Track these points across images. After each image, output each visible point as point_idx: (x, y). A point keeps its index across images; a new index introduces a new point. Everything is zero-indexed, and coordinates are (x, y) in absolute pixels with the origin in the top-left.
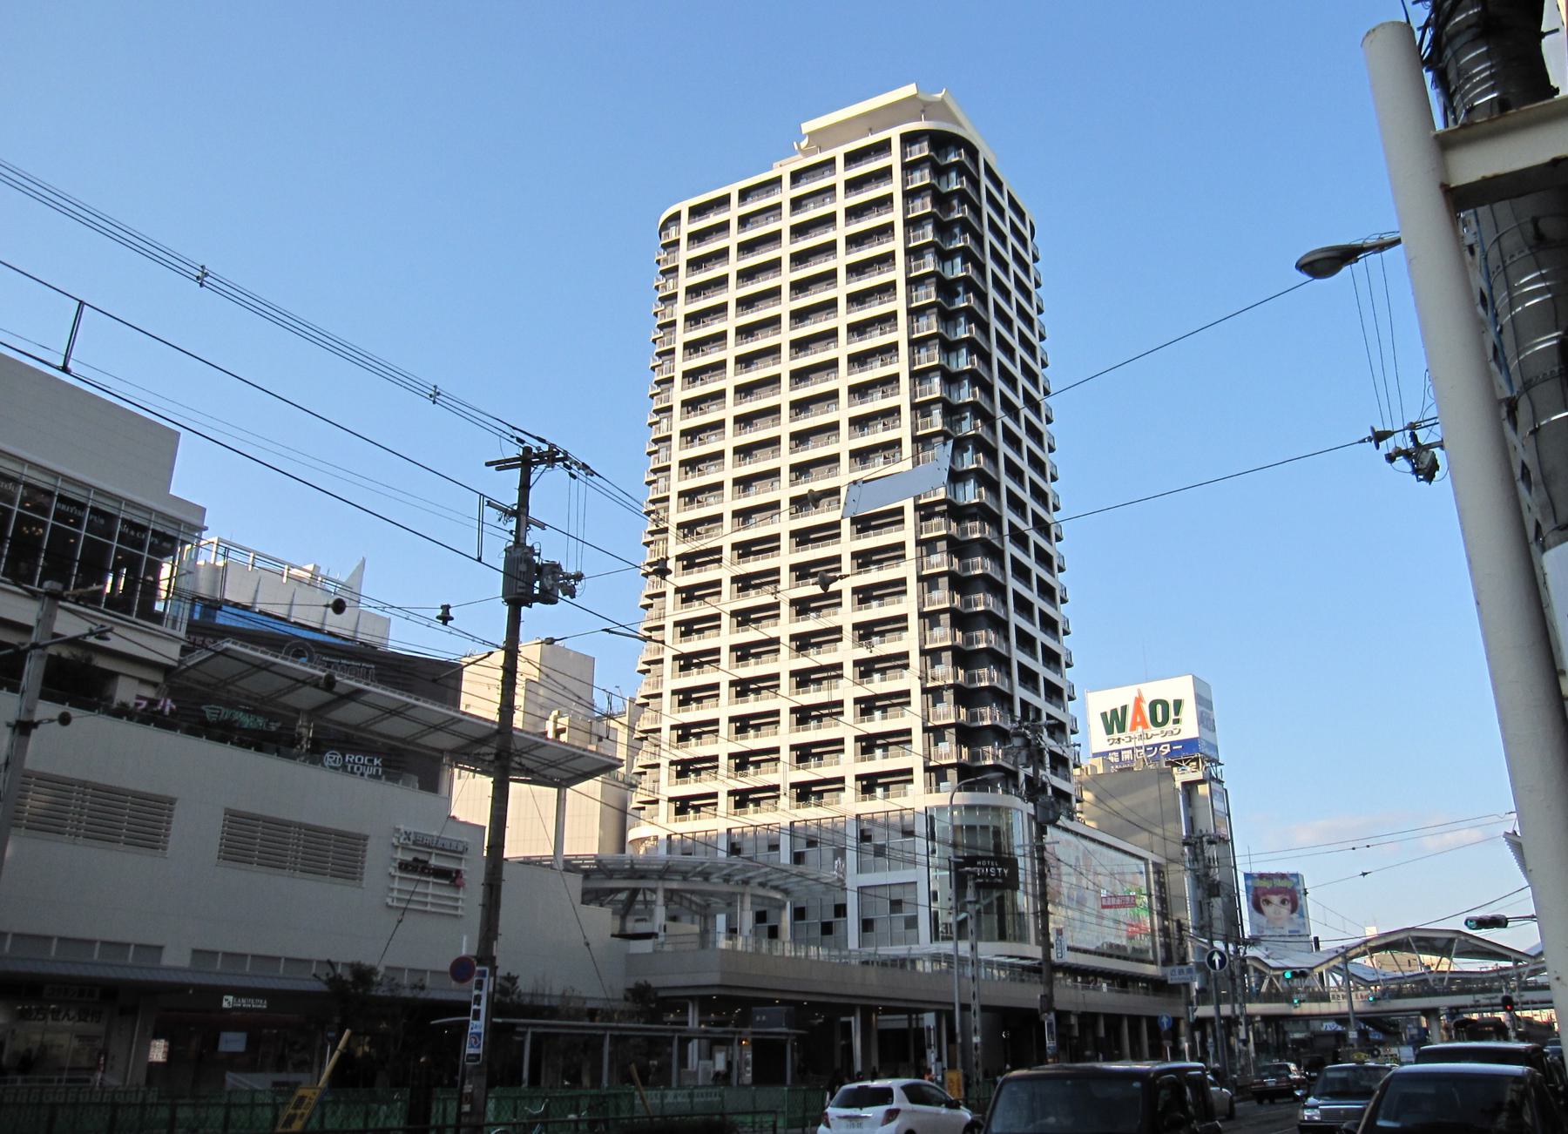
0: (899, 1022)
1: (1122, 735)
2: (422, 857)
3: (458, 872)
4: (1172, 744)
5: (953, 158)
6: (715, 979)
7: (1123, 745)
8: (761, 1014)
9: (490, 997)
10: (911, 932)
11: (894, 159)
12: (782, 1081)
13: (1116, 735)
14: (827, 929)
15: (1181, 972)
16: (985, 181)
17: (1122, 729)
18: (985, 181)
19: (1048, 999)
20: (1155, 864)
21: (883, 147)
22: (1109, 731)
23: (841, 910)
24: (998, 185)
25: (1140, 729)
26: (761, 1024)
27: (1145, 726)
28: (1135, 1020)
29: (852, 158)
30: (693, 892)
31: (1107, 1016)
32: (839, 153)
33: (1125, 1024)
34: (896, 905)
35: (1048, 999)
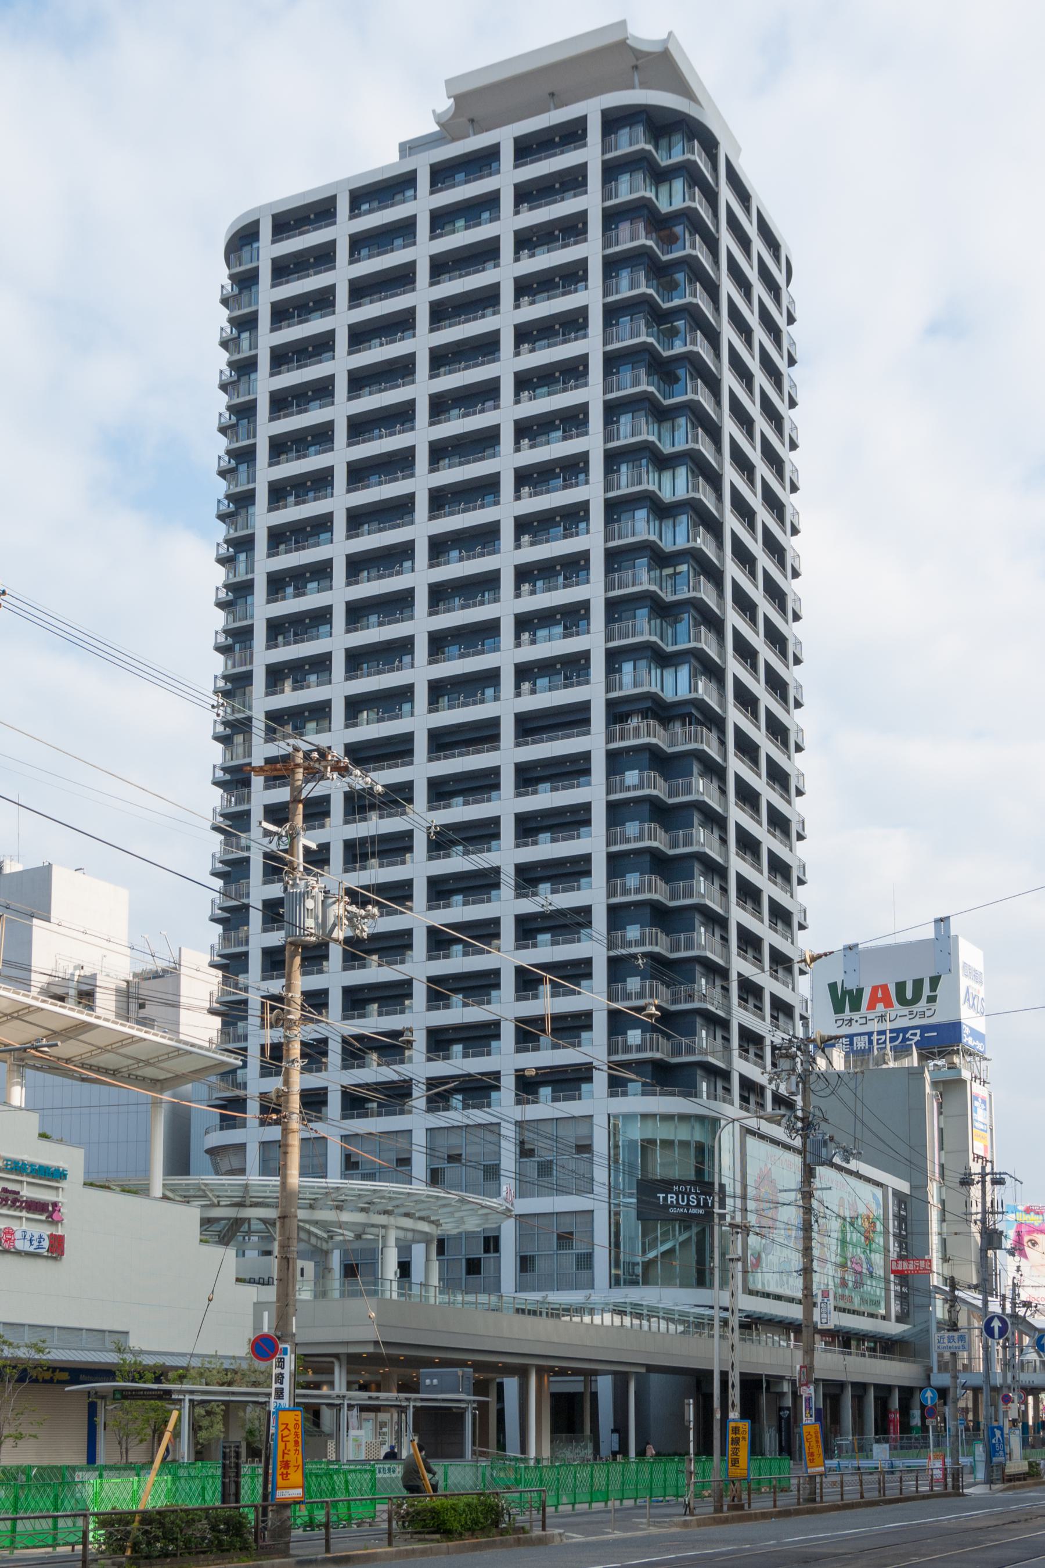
0: (573, 1385)
1: (855, 1016)
2: (11, 1187)
3: (55, 1205)
4: (924, 1029)
5: (678, 156)
6: (373, 1333)
7: (855, 1028)
8: (431, 1376)
9: (295, 1375)
10: (584, 1273)
11: (591, 154)
12: (461, 1455)
13: (847, 1014)
14: (473, 1267)
15: (951, 1339)
16: (726, 194)
17: (856, 1007)
18: (726, 194)
19: (808, 1368)
20: (897, 1193)
21: (572, 134)
22: (838, 1008)
23: (492, 1243)
24: (744, 196)
25: (880, 1007)
26: (432, 1389)
27: (888, 1004)
28: (861, 1388)
29: (527, 149)
30: (316, 1223)
31: (877, 1386)
32: (505, 137)
33: (849, 1392)
34: (565, 1239)
35: (808, 1368)
